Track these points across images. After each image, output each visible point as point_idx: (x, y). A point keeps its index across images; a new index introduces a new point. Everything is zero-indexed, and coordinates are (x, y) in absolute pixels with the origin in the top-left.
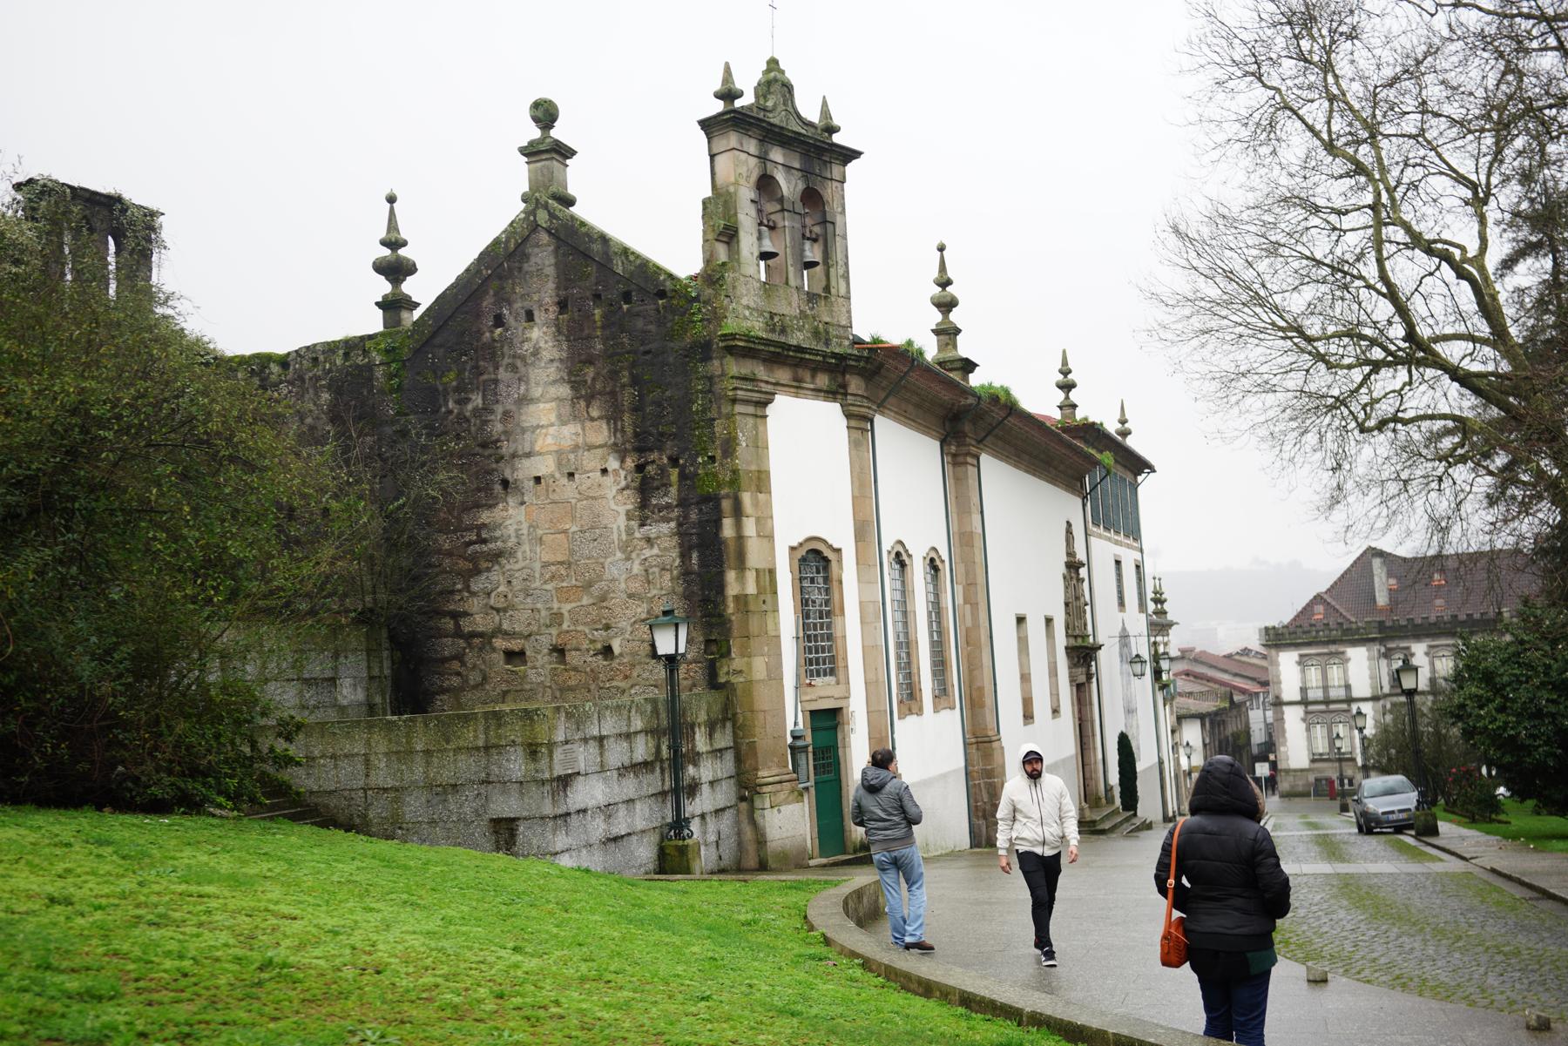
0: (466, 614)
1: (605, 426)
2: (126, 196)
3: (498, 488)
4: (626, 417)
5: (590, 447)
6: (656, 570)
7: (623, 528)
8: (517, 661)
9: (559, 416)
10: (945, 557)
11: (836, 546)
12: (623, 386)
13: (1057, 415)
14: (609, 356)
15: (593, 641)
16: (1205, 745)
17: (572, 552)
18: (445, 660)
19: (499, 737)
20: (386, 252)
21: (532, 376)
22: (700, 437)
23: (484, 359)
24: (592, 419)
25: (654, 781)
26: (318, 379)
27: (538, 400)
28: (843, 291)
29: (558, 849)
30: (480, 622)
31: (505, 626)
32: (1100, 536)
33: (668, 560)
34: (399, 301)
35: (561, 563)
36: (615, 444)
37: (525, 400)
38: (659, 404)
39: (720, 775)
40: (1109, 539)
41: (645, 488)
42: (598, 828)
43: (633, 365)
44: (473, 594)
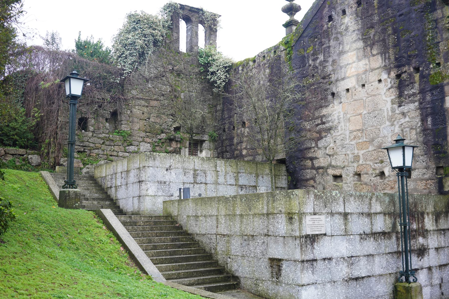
0: (316, 158)
2: (205, 9)
3: (330, 97)
4: (391, 51)
5: (372, 70)
6: (408, 129)
7: (389, 109)
8: (339, 180)
9: (358, 57)
12: (389, 35)
14: (381, 21)
15: (374, 169)
17: (364, 124)
18: (307, 180)
19: (274, 208)
21: (345, 41)
22: (431, 53)
23: (324, 38)
24: (374, 55)
25: (392, 244)
27: (348, 51)
29: (304, 283)
30: (322, 162)
33: (414, 124)
35: (359, 130)
36: (385, 66)
37: (341, 53)
38: (408, 41)
39: (443, 244)
41: (401, 86)
42: (343, 271)
43: (394, 23)
44: (319, 148)
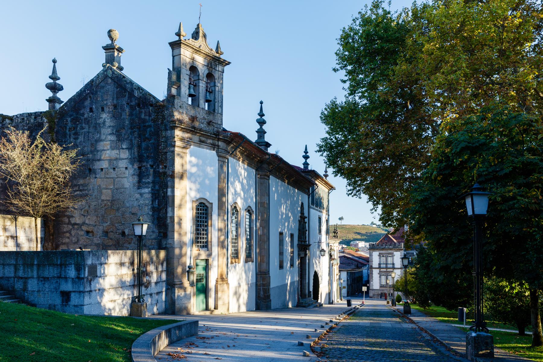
0: (72, 217)
1: (127, 152)
3: (87, 172)
9: (111, 147)
10: (254, 210)
11: (210, 202)
13: (302, 167)
16: (347, 280)
20: (52, 81)
21: (102, 132)
24: (123, 149)
26: (23, 126)
28: (220, 112)
31: (86, 222)
32: (314, 209)
34: (54, 100)
37: (99, 140)
40: (317, 210)
41: (141, 175)
